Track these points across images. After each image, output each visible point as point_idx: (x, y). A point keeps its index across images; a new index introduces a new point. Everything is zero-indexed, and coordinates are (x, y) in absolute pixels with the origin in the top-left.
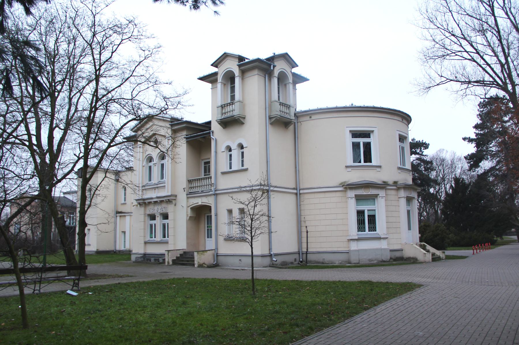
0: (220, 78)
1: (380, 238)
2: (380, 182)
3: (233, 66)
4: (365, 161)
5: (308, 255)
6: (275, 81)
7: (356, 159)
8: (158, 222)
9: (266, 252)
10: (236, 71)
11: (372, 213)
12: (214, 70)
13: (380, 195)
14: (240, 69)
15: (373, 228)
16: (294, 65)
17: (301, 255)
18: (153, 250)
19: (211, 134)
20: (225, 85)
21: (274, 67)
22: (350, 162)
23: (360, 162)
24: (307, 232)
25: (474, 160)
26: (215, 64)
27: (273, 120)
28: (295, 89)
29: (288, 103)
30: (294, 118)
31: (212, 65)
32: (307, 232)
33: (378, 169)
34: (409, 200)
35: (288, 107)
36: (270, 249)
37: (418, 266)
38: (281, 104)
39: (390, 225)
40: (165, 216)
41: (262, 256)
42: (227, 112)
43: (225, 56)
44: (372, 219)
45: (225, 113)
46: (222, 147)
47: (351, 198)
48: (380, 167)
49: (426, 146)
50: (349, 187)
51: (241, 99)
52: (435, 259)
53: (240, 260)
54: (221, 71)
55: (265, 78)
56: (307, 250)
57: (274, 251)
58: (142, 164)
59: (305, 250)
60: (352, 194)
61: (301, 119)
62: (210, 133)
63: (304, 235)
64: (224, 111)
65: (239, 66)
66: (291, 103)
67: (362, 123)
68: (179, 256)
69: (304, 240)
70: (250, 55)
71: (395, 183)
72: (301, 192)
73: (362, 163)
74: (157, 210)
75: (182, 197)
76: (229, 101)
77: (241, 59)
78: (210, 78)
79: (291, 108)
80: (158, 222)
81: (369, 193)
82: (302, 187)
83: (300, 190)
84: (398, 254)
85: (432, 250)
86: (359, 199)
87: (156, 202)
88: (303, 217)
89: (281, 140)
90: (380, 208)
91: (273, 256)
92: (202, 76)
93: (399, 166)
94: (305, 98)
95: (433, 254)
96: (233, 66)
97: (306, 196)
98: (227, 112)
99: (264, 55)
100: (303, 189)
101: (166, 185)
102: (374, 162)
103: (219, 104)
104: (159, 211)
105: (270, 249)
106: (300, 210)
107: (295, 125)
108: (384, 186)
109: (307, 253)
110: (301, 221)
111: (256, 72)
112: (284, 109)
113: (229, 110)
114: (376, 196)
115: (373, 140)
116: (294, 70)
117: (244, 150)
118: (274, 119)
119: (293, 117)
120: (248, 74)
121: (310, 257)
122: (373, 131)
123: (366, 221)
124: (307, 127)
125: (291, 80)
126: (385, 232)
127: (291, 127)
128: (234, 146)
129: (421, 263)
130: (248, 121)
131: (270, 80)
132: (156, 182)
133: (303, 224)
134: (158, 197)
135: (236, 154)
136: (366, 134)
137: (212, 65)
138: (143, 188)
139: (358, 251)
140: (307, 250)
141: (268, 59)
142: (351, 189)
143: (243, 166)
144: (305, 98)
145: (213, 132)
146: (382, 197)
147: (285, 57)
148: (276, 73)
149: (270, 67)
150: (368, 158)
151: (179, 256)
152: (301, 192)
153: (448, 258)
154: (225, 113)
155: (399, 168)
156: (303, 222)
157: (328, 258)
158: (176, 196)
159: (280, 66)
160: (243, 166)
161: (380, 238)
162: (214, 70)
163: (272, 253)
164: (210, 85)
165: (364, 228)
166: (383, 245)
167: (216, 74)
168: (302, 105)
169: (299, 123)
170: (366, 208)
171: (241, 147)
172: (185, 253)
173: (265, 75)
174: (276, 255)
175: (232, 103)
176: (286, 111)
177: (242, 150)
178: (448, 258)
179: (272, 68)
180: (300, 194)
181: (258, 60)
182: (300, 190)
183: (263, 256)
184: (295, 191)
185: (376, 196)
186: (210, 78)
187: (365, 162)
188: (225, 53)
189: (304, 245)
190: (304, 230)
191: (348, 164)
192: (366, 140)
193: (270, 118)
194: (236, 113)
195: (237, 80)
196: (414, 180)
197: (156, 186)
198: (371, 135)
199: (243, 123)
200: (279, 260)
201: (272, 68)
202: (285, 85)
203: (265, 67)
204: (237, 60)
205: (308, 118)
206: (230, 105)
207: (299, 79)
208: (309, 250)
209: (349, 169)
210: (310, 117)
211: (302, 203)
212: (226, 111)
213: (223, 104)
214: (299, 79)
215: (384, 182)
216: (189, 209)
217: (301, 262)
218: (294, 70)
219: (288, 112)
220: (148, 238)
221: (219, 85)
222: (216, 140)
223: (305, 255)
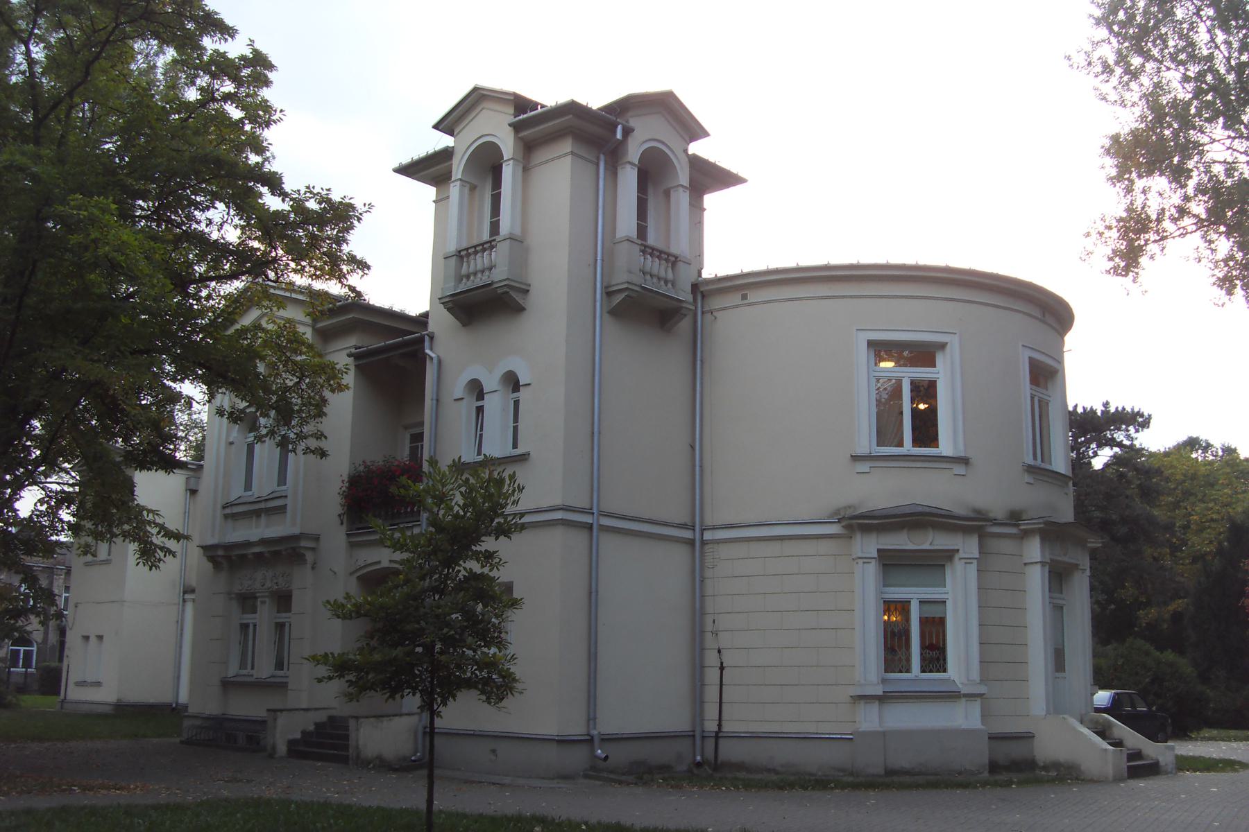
0: (458, 168)
1: (952, 696)
2: (961, 512)
3: (496, 128)
4: (917, 442)
5: (721, 742)
6: (628, 179)
7: (887, 431)
8: (264, 616)
9: (577, 729)
10: (508, 145)
11: (933, 612)
12: (446, 141)
13: (961, 554)
14: (517, 139)
15: (935, 657)
16: (694, 130)
17: (698, 742)
18: (247, 707)
19: (427, 344)
20: (473, 188)
21: (627, 132)
22: (865, 441)
23: (901, 444)
24: (722, 668)
25: (1172, 7)
26: (446, 124)
27: (618, 298)
28: (697, 208)
29: (674, 250)
30: (690, 298)
31: (436, 127)
32: (722, 668)
33: (959, 469)
34: (1058, 576)
35: (673, 260)
36: (591, 719)
37: (1039, 781)
38: (647, 250)
39: (998, 656)
40: (283, 600)
41: (559, 742)
42: (475, 274)
43: (477, 98)
44: (934, 628)
45: (468, 277)
46: (458, 387)
47: (866, 560)
48: (964, 461)
49: (1138, 420)
50: (859, 523)
51: (962, 454)
52: (1141, 768)
53: (494, 751)
54: (460, 144)
55: (598, 165)
56: (720, 725)
57: (609, 724)
58: (228, 435)
59: (711, 726)
60: (869, 545)
61: (716, 303)
62: (421, 341)
63: (712, 676)
64: (464, 271)
65: (517, 127)
66: (679, 246)
67: (910, 320)
68: (312, 728)
69: (712, 693)
70: (549, 95)
71: (1015, 517)
72: (708, 536)
73: (908, 447)
74: (261, 580)
75: (335, 537)
76: (486, 236)
77: (521, 104)
78: (426, 169)
79: (681, 265)
80: (264, 616)
81: (926, 546)
82: (709, 522)
83: (702, 531)
84: (1016, 751)
85: (1133, 739)
86: (891, 563)
87: (259, 556)
88: (709, 619)
89: (644, 365)
90: (958, 594)
91: (596, 740)
92: (406, 160)
93: (1032, 463)
94: (732, 240)
95: (1136, 755)
96: (496, 128)
97: (724, 551)
98: (475, 274)
99: (597, 96)
100: (714, 528)
101: (289, 502)
102: (946, 445)
103: (452, 247)
104: (268, 584)
105: (591, 719)
106: (702, 596)
107: (695, 322)
108: (975, 524)
109: (717, 736)
110: (702, 632)
111: (567, 146)
112: (655, 266)
113: (479, 267)
114: (950, 555)
115: (942, 372)
116: (695, 148)
117: (523, 394)
118: (623, 296)
119: (685, 295)
120: (541, 155)
121: (729, 751)
122: (942, 346)
123: (913, 643)
124: (730, 327)
125: (683, 177)
126: (975, 675)
127: (684, 325)
128: (491, 382)
129: (1092, 781)
130: (534, 302)
131: (613, 171)
132: (265, 493)
133: (710, 641)
134: (263, 542)
135: (495, 404)
136: (924, 354)
137: (436, 127)
138: (228, 511)
139: (884, 734)
140: (720, 725)
141: (609, 108)
142: (866, 529)
143: (515, 446)
144: (732, 240)
145: (432, 338)
146: (968, 561)
147: (665, 106)
148: (634, 152)
149: (615, 133)
150: (926, 429)
151: (312, 728)
152: (708, 536)
153: (1186, 764)
154: (468, 277)
155: (1030, 469)
156: (708, 636)
157: (782, 755)
158: (317, 538)
159: (644, 134)
160: (515, 446)
161: (952, 696)
162: (446, 141)
163: (594, 732)
164: (430, 192)
165: (908, 660)
166: (965, 717)
167: (444, 155)
168: (719, 260)
169: (708, 316)
170: (914, 593)
171: (512, 382)
172: (331, 718)
173: (598, 158)
174: (607, 740)
175: (488, 246)
176: (662, 274)
177: (516, 395)
178: (1186, 764)
179: (619, 136)
180: (704, 543)
181: (572, 109)
182: (702, 531)
183: (563, 742)
184: (687, 534)
185: (950, 555)
186: (426, 169)
187: (923, 671)
188: (476, 89)
189: (711, 712)
190: (711, 659)
191: (863, 449)
192: (922, 373)
193: (609, 294)
194: (499, 275)
195: (508, 172)
196: (1079, 507)
197: (262, 506)
198: (940, 359)
199: (520, 309)
200: (621, 755)
201: (619, 136)
202: (667, 194)
203: (596, 133)
204: (512, 111)
205: (735, 299)
206: (484, 250)
207: (711, 177)
208: (727, 727)
209: (864, 467)
210: (744, 297)
211: (708, 573)
212: (472, 269)
213: (465, 246)
214: (711, 177)
215: (978, 511)
216: (353, 579)
217: (699, 765)
218: (695, 148)
219: (670, 276)
220: (233, 670)
221: (454, 190)
222: (440, 362)
223: (710, 744)
